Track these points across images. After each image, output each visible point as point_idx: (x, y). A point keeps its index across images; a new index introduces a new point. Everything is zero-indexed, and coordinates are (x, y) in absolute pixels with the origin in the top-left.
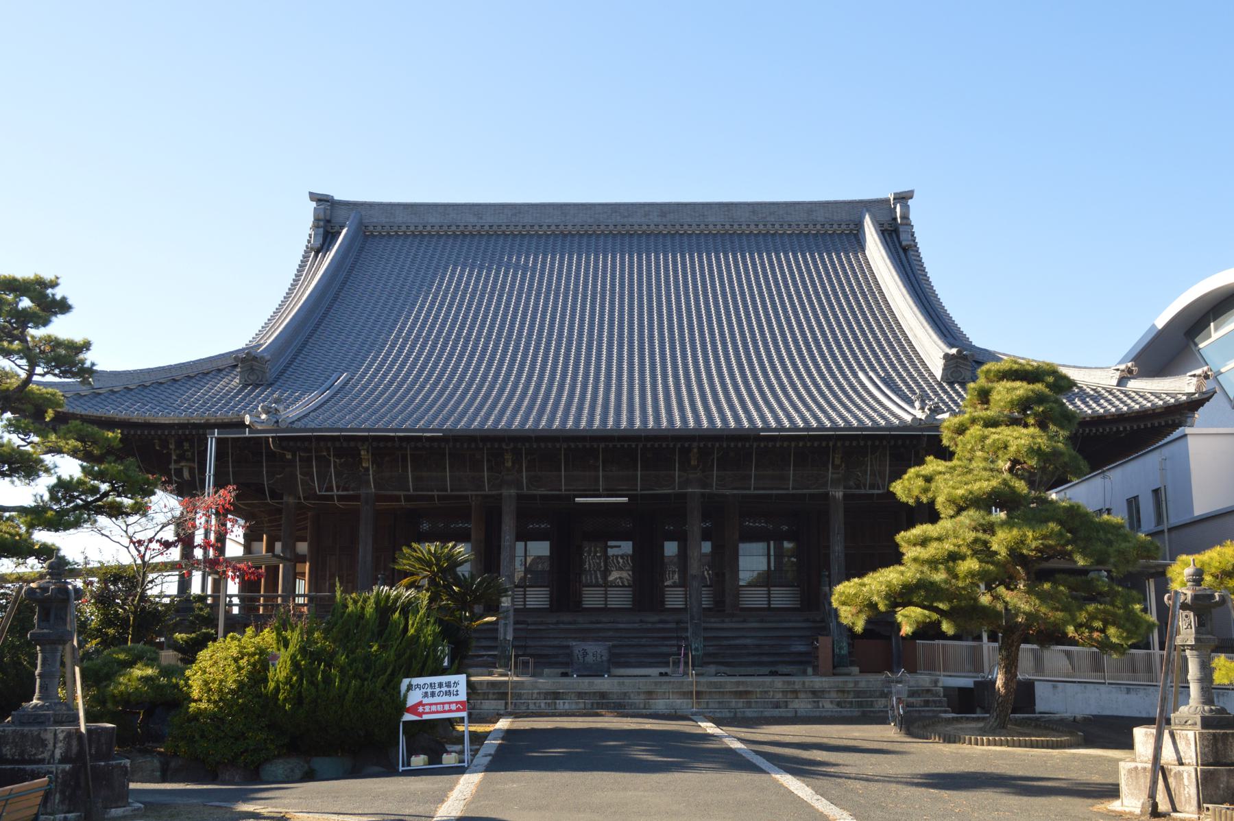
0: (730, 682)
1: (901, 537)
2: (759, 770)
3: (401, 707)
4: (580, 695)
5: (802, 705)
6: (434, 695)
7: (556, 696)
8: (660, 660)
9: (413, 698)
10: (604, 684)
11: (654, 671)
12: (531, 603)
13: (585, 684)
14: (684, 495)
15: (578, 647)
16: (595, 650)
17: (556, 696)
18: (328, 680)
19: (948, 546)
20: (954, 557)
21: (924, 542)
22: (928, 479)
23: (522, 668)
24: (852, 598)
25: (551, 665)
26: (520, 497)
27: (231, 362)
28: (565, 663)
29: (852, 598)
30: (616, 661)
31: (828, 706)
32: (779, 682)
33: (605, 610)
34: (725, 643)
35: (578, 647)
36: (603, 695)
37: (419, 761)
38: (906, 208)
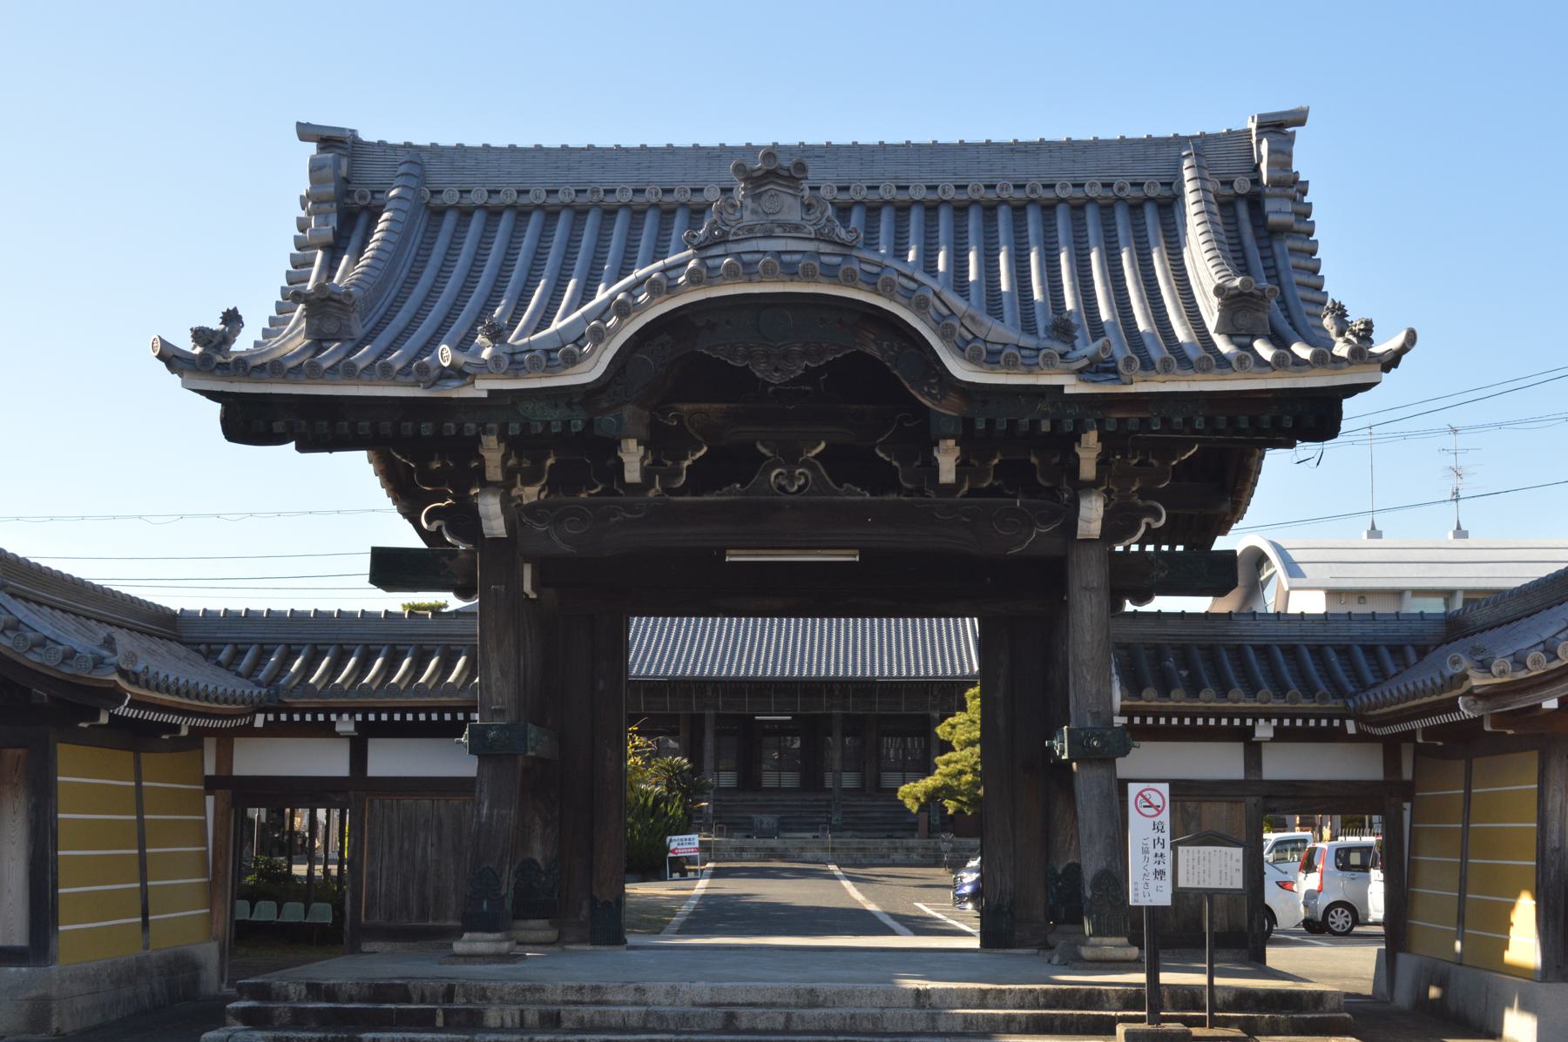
0: (855, 842)
1: (938, 759)
2: (895, 917)
3: (667, 850)
4: (757, 849)
5: (897, 857)
6: (684, 844)
7: (742, 850)
8: (813, 827)
9: (673, 846)
10: (774, 842)
11: (809, 835)
12: (723, 784)
13: (761, 843)
14: (830, 715)
15: (757, 817)
16: (768, 820)
17: (742, 850)
18: (633, 837)
19: (959, 766)
20: (961, 773)
21: (947, 763)
22: (953, 727)
23: (720, 833)
24: (911, 792)
25: (739, 830)
26: (718, 716)
27: (254, 375)
28: (747, 828)
29: (911, 792)
30: (784, 827)
31: (915, 857)
32: (886, 842)
33: (780, 790)
34: (386, 849)
35: (757, 817)
36: (772, 849)
37: (676, 875)
38: (1282, 156)
